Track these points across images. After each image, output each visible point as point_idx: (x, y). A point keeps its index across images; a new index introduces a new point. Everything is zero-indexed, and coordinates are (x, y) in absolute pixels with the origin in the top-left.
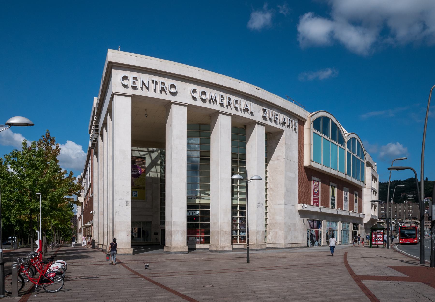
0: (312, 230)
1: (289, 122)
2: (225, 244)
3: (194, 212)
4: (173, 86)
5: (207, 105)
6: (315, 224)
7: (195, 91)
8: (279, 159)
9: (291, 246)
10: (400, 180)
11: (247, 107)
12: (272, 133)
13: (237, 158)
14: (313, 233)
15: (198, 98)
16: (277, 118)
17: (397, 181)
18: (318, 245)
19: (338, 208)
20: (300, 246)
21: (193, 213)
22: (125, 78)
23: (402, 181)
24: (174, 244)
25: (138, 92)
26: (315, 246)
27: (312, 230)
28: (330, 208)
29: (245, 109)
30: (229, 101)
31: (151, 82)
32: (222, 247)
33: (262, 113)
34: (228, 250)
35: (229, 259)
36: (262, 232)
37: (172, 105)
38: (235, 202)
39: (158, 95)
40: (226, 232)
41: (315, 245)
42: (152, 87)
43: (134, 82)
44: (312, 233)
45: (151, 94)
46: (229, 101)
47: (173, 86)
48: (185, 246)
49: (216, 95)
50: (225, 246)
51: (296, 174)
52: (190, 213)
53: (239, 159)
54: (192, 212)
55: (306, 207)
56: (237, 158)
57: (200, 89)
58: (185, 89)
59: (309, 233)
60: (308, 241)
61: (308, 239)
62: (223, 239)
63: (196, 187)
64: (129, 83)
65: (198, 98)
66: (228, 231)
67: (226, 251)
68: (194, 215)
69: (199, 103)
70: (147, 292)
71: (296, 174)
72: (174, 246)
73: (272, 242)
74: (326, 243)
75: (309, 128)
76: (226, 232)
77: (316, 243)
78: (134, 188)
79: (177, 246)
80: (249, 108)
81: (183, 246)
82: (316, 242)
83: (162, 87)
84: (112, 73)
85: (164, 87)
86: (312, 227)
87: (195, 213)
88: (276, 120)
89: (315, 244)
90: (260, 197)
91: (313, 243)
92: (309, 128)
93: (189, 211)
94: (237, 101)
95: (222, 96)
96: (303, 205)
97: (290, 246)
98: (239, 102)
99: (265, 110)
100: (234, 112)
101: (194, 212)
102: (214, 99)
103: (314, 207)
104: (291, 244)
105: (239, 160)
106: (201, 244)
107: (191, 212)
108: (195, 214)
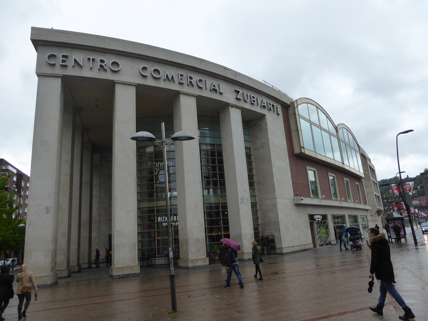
1: (269, 106)
2: (197, 256)
4: (115, 64)
5: (162, 84)
7: (144, 68)
10: (386, 179)
11: (215, 87)
13: (214, 150)
16: (254, 101)
17: (384, 180)
22: (52, 56)
23: (388, 179)
25: (71, 72)
28: (335, 244)
29: (212, 89)
30: (191, 80)
31: (86, 59)
33: (234, 95)
37: (116, 85)
38: (425, 221)
39: (96, 74)
40: (197, 239)
42: (87, 65)
43: (63, 61)
45: (86, 73)
46: (191, 80)
47: (115, 64)
48: (135, 265)
49: (173, 74)
50: (197, 260)
51: (286, 163)
56: (214, 149)
57: (151, 67)
63: (224, 195)
64: (59, 61)
69: (150, 82)
71: (286, 163)
72: (118, 266)
74: (336, 240)
81: (132, 265)
83: (100, 65)
84: (115, 95)
85: (103, 64)
88: (253, 102)
90: (243, 191)
94: (200, 81)
98: (203, 81)
99: (238, 92)
100: (198, 92)
102: (170, 78)
103: (314, 200)
104: (292, 247)
106: (158, 258)
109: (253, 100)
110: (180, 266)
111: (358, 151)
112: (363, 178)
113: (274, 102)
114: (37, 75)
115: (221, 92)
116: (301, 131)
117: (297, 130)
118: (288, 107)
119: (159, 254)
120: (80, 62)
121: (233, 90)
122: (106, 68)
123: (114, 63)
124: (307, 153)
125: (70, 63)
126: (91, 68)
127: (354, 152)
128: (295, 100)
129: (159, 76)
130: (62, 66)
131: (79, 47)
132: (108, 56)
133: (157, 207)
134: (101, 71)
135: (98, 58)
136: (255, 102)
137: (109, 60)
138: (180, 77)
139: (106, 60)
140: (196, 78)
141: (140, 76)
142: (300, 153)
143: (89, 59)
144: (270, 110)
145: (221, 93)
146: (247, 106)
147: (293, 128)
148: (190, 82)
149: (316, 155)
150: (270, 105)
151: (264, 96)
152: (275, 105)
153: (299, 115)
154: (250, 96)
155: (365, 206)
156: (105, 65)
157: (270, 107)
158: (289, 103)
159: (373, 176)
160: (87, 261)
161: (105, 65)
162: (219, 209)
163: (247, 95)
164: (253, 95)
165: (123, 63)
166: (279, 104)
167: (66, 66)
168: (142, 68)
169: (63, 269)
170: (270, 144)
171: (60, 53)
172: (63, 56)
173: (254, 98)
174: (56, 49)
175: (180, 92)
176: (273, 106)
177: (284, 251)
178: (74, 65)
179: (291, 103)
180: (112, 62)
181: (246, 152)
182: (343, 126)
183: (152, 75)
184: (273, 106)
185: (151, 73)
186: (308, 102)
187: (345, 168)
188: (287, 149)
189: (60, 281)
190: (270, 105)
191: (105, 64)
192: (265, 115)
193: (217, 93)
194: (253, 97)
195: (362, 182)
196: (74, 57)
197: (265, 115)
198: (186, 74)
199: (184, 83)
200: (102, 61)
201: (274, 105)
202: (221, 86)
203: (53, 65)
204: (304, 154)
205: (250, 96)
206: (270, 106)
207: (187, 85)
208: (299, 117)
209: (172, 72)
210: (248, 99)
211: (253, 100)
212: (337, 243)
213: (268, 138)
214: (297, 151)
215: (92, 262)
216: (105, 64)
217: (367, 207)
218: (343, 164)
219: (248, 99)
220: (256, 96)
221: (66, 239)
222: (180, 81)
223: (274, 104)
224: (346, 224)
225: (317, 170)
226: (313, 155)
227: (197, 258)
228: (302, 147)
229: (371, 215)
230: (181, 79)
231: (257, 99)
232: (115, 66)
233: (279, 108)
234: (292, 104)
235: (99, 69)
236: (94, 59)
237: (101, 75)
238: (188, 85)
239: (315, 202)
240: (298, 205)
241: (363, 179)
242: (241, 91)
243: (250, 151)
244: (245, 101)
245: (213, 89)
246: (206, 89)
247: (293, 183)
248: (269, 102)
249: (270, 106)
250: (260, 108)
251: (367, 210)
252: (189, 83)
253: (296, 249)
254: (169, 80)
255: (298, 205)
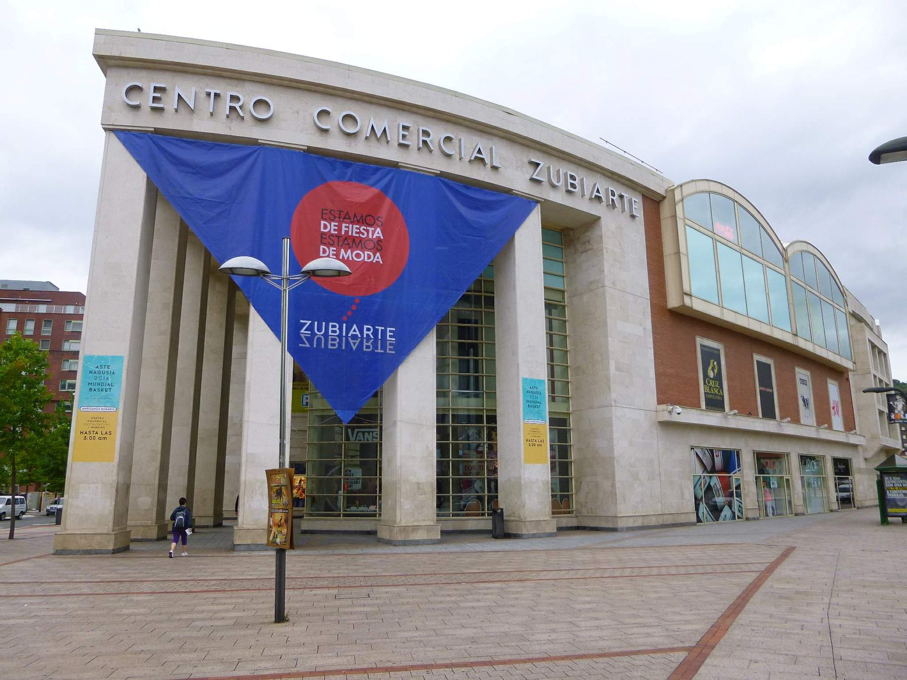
0: (711, 477)
1: (611, 197)
3: (369, 432)
6: (718, 461)
7: (324, 113)
8: (592, 290)
9: (643, 523)
12: (573, 230)
14: (712, 484)
15: (334, 131)
16: (573, 185)
18: (734, 517)
19: (782, 418)
20: (673, 523)
21: (366, 435)
24: (245, 522)
26: (724, 520)
27: (711, 477)
29: (473, 158)
31: (204, 95)
32: (405, 529)
34: (425, 537)
35: (326, 583)
36: (543, 482)
40: (418, 484)
41: (721, 520)
43: (155, 99)
44: (709, 484)
45: (202, 125)
50: (415, 528)
52: (358, 436)
53: (484, 292)
54: (363, 433)
55: (679, 414)
57: (338, 109)
58: (297, 112)
59: (699, 483)
60: (697, 509)
61: (697, 501)
62: (408, 507)
65: (334, 131)
66: (424, 481)
67: (416, 543)
68: (368, 440)
70: (443, 606)
71: (644, 328)
73: (588, 513)
75: (674, 214)
76: (421, 486)
77: (726, 511)
78: (305, 388)
79: (255, 527)
80: (485, 155)
82: (726, 508)
83: (231, 108)
85: (237, 106)
86: (709, 468)
87: (371, 433)
88: (570, 188)
89: (723, 514)
91: (716, 511)
92: (673, 216)
93: (356, 430)
94: (448, 139)
95: (405, 128)
96: (671, 407)
97: (639, 523)
98: (455, 141)
101: (369, 432)
102: (379, 134)
103: (707, 415)
105: (483, 294)
107: (361, 433)
108: (370, 438)
109: (570, 183)
110: (381, 537)
111: (843, 306)
112: (852, 371)
113: (625, 187)
114: (103, 128)
115: (495, 164)
116: (687, 255)
117: (678, 253)
118: (660, 201)
119: (839, 478)
120: (189, 99)
121: (526, 160)
122: (242, 114)
123: (259, 103)
124: (698, 306)
125: (170, 103)
126: (212, 114)
127: (828, 310)
128: (678, 186)
129: (355, 129)
130: (154, 109)
131: (180, 67)
132: (249, 87)
133: (453, 409)
134: (232, 119)
135: (227, 90)
136: (575, 188)
137: (248, 95)
138: (402, 132)
139: (269, 98)
140: (438, 133)
141: (314, 130)
142: (681, 306)
143: (209, 94)
144: (613, 205)
145: (495, 168)
146: (558, 197)
147: (668, 249)
148: (425, 142)
149: (722, 314)
150: (613, 195)
151: (599, 175)
152: (625, 195)
153: (685, 218)
154: (566, 174)
155: (847, 436)
156: (241, 107)
157: (612, 200)
158: (662, 192)
159: (881, 366)
160: (211, 512)
161: (241, 107)
162: (482, 422)
163: (558, 171)
164: (573, 171)
165: (277, 100)
166: (637, 194)
167: (161, 110)
168: (318, 114)
169: (149, 523)
170: (607, 283)
171: (148, 82)
172: (156, 89)
173: (575, 180)
174: (144, 74)
175: (400, 164)
176: (621, 197)
177: (621, 524)
178: (228, 113)
179: (666, 191)
180: (344, 114)
181: (545, 299)
182: (805, 247)
183: (340, 130)
184: (621, 197)
185: (339, 125)
186: (712, 189)
187: (798, 346)
188: (648, 297)
189: (133, 546)
190: (612, 195)
191: (240, 103)
192: (599, 218)
193: (486, 166)
194: (572, 177)
195: (848, 380)
196: (178, 90)
197: (599, 218)
198: (417, 124)
199: (410, 145)
200: (234, 98)
201: (624, 196)
202: (496, 153)
203: (136, 108)
204: (691, 309)
205: (566, 174)
206: (613, 198)
207: (416, 148)
208: (685, 224)
209: (382, 120)
210: (559, 181)
211: (570, 183)
212: (760, 517)
213: (604, 271)
214: (673, 302)
215: (224, 517)
216: (240, 103)
217: (853, 440)
218: (796, 335)
219: (559, 181)
220: (580, 174)
221: (157, 464)
222: (401, 141)
223: (622, 194)
224: (792, 475)
225: (725, 347)
226: (713, 311)
227: (416, 524)
228: (687, 294)
229: (865, 457)
230: (404, 136)
231: (582, 180)
232: (262, 108)
233: (635, 202)
234: (670, 192)
235: (227, 115)
236: (219, 94)
237: (230, 129)
238: (419, 149)
239: (713, 419)
240: (667, 425)
241: (850, 373)
242: (542, 164)
243: (563, 298)
244: (554, 186)
245: (476, 157)
246: (460, 159)
247: (658, 375)
248: (610, 188)
249: (613, 198)
250: (588, 201)
251: (855, 446)
252: (421, 146)
253: (653, 521)
254: (378, 140)
255: (667, 425)
